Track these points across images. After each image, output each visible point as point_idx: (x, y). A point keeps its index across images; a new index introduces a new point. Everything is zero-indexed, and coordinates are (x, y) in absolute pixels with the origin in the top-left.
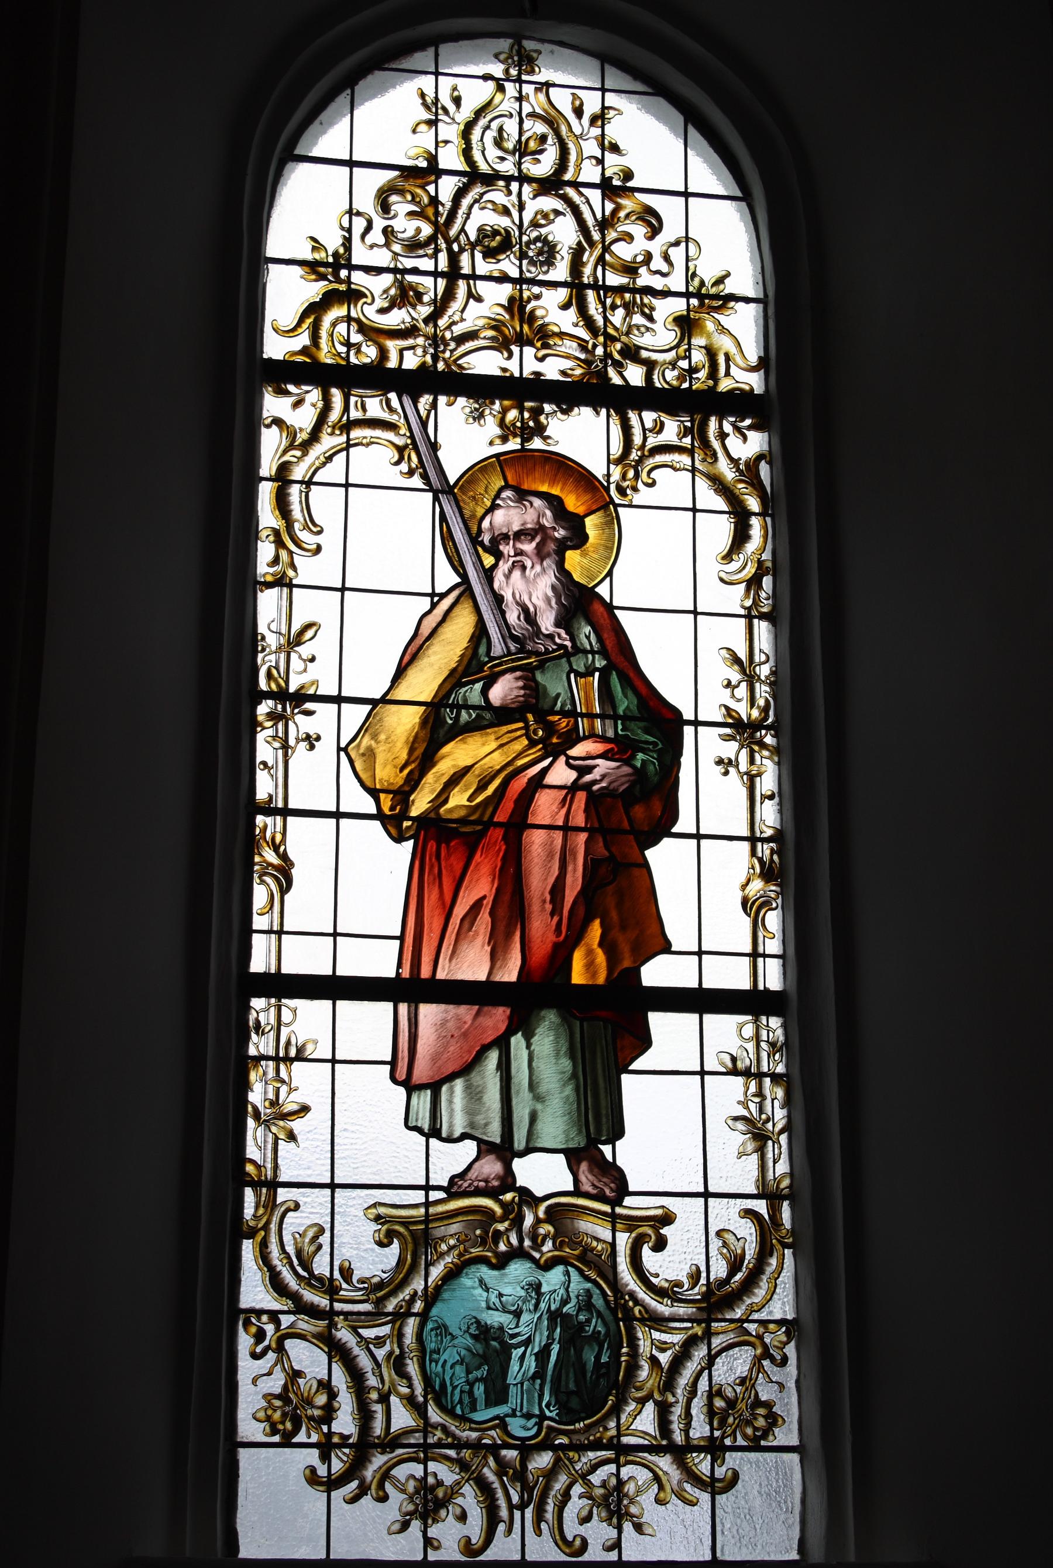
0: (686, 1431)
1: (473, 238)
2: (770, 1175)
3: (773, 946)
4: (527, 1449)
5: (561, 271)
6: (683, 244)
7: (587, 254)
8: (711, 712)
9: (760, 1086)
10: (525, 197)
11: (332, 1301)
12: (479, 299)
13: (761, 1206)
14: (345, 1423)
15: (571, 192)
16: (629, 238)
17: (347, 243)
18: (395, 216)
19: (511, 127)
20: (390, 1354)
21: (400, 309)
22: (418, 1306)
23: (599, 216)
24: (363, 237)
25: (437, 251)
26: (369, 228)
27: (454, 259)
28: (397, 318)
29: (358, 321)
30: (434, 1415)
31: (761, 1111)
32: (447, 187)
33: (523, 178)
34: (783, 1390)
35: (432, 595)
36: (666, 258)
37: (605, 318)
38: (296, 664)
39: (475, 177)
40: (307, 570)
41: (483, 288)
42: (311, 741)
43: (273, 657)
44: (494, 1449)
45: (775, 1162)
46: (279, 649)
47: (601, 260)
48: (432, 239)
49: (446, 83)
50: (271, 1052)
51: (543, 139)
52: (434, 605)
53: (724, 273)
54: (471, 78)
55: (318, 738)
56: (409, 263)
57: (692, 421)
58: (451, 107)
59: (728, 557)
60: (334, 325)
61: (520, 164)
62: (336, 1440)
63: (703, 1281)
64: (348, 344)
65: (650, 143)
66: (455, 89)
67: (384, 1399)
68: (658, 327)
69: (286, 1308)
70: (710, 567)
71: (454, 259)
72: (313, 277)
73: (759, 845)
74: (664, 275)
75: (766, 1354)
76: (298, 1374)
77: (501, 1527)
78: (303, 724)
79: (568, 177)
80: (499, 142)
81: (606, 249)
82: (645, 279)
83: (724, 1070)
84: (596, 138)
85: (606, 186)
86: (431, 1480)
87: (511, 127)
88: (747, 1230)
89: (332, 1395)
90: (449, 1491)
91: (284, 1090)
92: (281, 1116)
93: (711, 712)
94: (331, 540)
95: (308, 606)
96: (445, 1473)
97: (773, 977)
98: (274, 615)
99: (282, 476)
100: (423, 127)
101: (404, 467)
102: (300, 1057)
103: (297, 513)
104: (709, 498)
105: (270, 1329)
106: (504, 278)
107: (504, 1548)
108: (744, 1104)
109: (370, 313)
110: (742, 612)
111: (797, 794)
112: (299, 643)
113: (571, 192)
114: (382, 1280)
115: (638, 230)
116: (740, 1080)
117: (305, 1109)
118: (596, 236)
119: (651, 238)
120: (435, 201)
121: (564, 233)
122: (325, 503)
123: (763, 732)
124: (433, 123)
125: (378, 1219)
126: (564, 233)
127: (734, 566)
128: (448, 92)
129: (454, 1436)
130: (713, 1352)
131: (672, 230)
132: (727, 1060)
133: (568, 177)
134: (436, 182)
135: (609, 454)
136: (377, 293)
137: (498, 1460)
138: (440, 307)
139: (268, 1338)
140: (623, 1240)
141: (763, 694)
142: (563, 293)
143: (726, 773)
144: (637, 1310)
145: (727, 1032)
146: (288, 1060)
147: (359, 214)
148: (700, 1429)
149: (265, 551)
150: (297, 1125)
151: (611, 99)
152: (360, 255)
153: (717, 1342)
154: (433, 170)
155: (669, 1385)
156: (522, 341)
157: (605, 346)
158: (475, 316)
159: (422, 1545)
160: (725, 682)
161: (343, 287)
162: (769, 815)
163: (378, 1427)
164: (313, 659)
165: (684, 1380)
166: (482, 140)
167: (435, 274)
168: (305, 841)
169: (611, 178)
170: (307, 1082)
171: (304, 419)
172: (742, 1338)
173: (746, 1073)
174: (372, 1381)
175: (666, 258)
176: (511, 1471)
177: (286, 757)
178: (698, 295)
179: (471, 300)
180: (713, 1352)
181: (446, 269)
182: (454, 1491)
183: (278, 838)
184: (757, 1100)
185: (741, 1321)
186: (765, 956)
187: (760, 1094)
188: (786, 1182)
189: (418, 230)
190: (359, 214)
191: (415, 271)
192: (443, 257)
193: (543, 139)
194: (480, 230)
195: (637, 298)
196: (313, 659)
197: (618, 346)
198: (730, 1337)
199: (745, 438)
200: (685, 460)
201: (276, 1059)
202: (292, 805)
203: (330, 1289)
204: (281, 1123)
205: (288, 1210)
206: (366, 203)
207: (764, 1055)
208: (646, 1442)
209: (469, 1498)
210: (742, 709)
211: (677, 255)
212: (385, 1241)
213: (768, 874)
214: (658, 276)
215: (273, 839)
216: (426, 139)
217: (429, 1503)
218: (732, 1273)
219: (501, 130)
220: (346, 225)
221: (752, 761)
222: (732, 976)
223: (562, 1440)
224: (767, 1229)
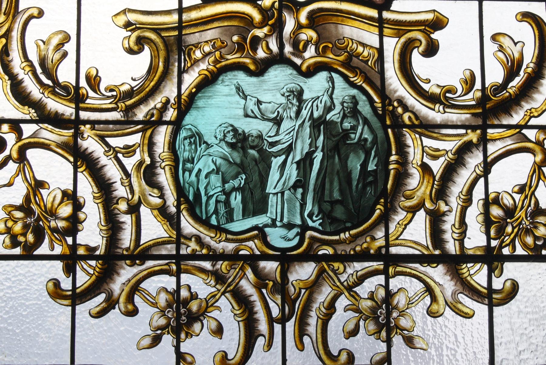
0: (461, 242)
20: (141, 163)
30: (188, 225)
44: (252, 260)
62: (81, 251)
67: (134, 209)
76: (40, 184)
77: (260, 342)
86: (184, 293)
89: (78, 206)
96: (199, 285)
114: (132, 88)
125: (128, 25)
130: (489, 160)
137: (256, 272)
140: (392, 46)
144: (406, 116)
148: (476, 239)
153: (493, 149)
155: (441, 194)
163: (126, 239)
174: (121, 191)
180: (489, 160)
182: (209, 304)
198: (509, 144)
203: (77, 98)
208: (417, 252)
209: (226, 312)
223: (327, 250)
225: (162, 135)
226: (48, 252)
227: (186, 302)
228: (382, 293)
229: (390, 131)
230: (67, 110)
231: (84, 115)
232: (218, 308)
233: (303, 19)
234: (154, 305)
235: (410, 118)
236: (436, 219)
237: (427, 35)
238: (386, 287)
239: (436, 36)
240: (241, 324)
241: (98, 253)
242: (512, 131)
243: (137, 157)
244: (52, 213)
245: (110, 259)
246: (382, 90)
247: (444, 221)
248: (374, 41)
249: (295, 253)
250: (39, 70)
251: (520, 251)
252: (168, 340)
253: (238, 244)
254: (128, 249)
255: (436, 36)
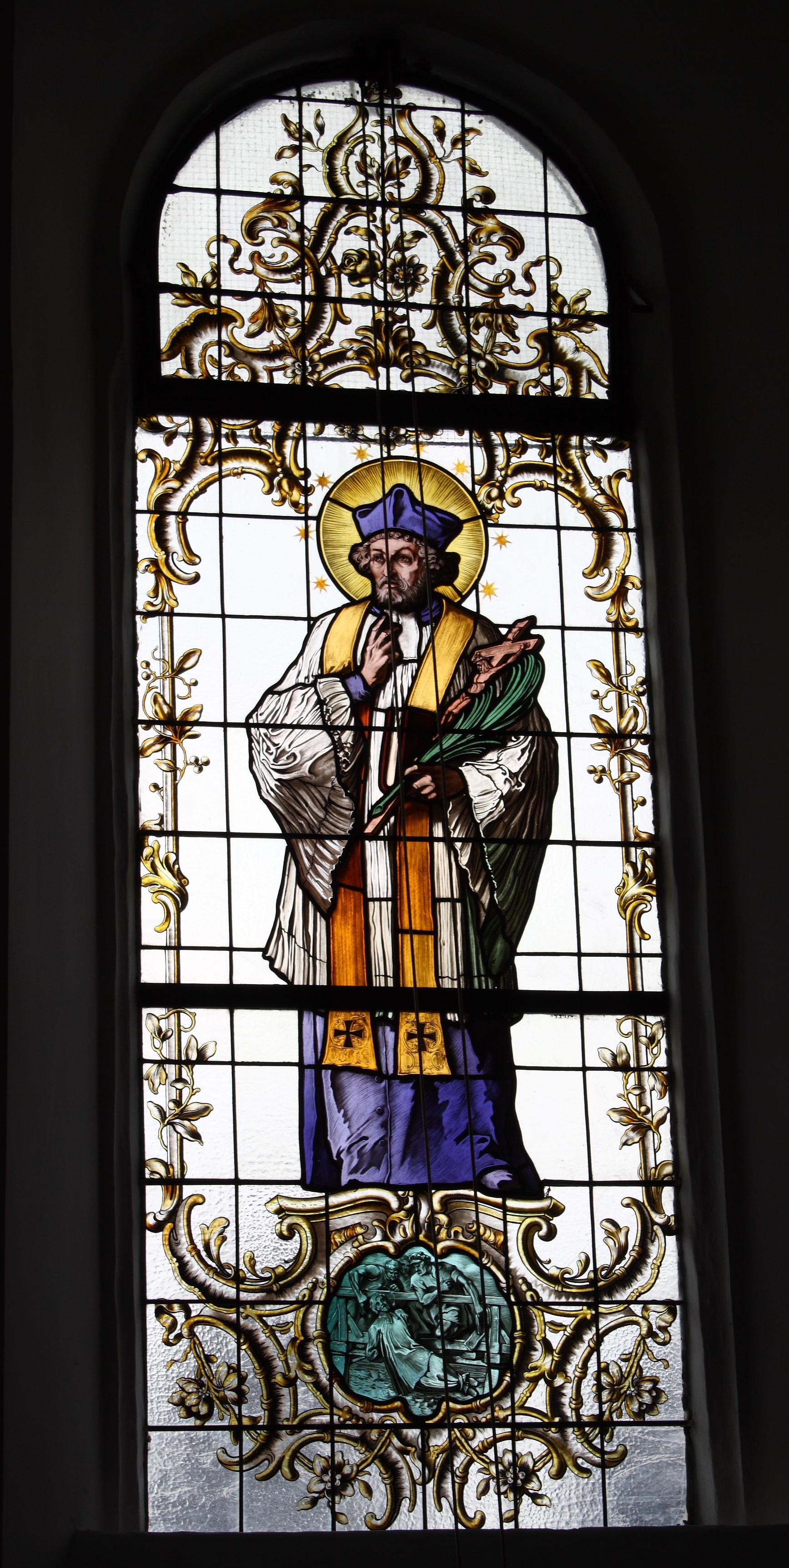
0: (577, 1410)
1: (339, 262)
2: (652, 1164)
3: (653, 945)
4: (427, 1431)
5: (424, 295)
6: (545, 263)
7: (451, 275)
8: (581, 723)
9: (640, 1078)
10: (388, 221)
11: (238, 1290)
12: (346, 322)
13: (638, 1193)
14: (254, 1409)
15: (431, 214)
16: (491, 259)
17: (216, 272)
18: (262, 243)
19: (374, 151)
20: (294, 1340)
21: (269, 331)
22: (320, 1295)
23: (461, 237)
24: (232, 262)
25: (304, 275)
26: (238, 251)
27: (320, 283)
28: (266, 340)
29: (230, 346)
30: (339, 1395)
31: (641, 1103)
32: (312, 213)
33: (386, 205)
34: (667, 1366)
35: (309, 618)
36: (528, 277)
37: (469, 338)
38: (181, 689)
39: (337, 201)
40: (186, 597)
41: (349, 310)
42: (200, 765)
43: (157, 683)
44: (396, 1429)
45: (655, 1152)
46: (163, 677)
47: (465, 280)
48: (299, 264)
49: (310, 109)
50: (174, 1056)
51: (407, 161)
52: (310, 629)
53: (585, 292)
54: (332, 108)
55: (207, 763)
56: (276, 288)
57: (553, 441)
58: (315, 134)
59: (589, 574)
60: (205, 348)
61: (383, 188)
62: (246, 1422)
63: (591, 1267)
64: (218, 364)
65: (508, 165)
66: (318, 115)
67: (291, 1383)
68: (521, 344)
69: (195, 1298)
70: (576, 584)
71: (320, 283)
72: (184, 302)
73: (633, 850)
74: (528, 294)
75: (651, 1334)
76: (209, 1359)
77: (406, 1504)
78: (189, 748)
79: (431, 200)
80: (362, 167)
81: (469, 268)
82: (507, 299)
83: (605, 1066)
84: (458, 160)
85: (466, 208)
86: (338, 1458)
87: (374, 151)
88: (630, 1220)
89: (242, 1379)
90: (355, 1468)
91: (186, 1092)
92: (184, 1116)
93: (581, 723)
94: (208, 568)
95: (189, 634)
96: (353, 1455)
97: (652, 979)
98: (157, 643)
99: (160, 508)
100: (287, 153)
101: (276, 495)
102: (202, 1059)
103: (174, 543)
104: (572, 515)
105: (180, 1317)
106: (371, 301)
107: (408, 1521)
108: (625, 1097)
109: (239, 335)
110: (610, 625)
111: (672, 800)
112: (181, 670)
113: (431, 214)
114: (286, 1270)
115: (500, 252)
116: (620, 1074)
117: (205, 1110)
118: (459, 257)
119: (513, 257)
120: (300, 227)
121: (427, 253)
122: (201, 532)
123: (634, 741)
124: (297, 150)
125: (280, 1211)
126: (427, 253)
127: (599, 581)
128: (312, 120)
129: (358, 1418)
130: (601, 1331)
131: (533, 250)
132: (609, 1057)
133: (431, 200)
134: (302, 208)
135: (473, 475)
136: (247, 316)
137: (403, 1439)
138: (309, 327)
139: (179, 1327)
140: (515, 1232)
141: (631, 705)
142: (427, 315)
143: (600, 781)
144: (529, 1294)
145: (607, 1032)
146: (189, 1063)
147: (226, 240)
148: (590, 1409)
149: (145, 582)
150: (200, 1125)
151: (472, 121)
152: (229, 281)
153: (603, 1323)
154: (299, 197)
155: (560, 1368)
156: (388, 362)
157: (469, 365)
158: (342, 335)
159: (330, 1519)
160: (595, 693)
161: (214, 312)
162: (644, 821)
163: (286, 1408)
164: (196, 684)
165: (576, 1359)
166: (346, 164)
167: (302, 298)
168: (199, 860)
169: (472, 199)
170: (209, 1084)
171: (179, 450)
172: (627, 1318)
173: (624, 1068)
174: (279, 1365)
175: (528, 277)
176: (413, 1449)
177: (175, 778)
178: (560, 315)
179: (338, 322)
180: (601, 1331)
181: (313, 293)
182: (360, 1469)
183: (172, 858)
184: (637, 1092)
185: (628, 1302)
186: (642, 955)
187: (640, 1086)
188: (669, 1169)
189: (285, 256)
190: (226, 240)
191: (283, 296)
192: (309, 281)
193: (407, 161)
194: (346, 256)
195: (502, 317)
196: (196, 684)
197: (483, 364)
198: (620, 1318)
199: (605, 457)
200: (549, 480)
201: (179, 1062)
202: (643, 952)
203: (238, 1279)
204: (186, 1123)
205: (195, 1204)
206: (233, 229)
207: (643, 1048)
208: (539, 1421)
209: (374, 1476)
210: (612, 719)
211: (538, 274)
212: (285, 1233)
213: (641, 877)
214: (520, 296)
215: (167, 859)
216: (291, 165)
217: (338, 1481)
218: (619, 1260)
219: (364, 155)
220: (214, 251)
221: (623, 770)
222: (609, 977)
223: (461, 1419)
224: (645, 1210)
225: (316, 1312)
226: (219, 1423)
227: (341, 1466)
228: (509, 1457)
229: (515, 1308)
230: (230, 1291)
231: (244, 1296)
232: (369, 1474)
233: (437, 1206)
234: (312, 1469)
235: (532, 1296)
236: (555, 1395)
237: (548, 1221)
238: (513, 1451)
239: (556, 1221)
240: (388, 1486)
241: (261, 1424)
242: (621, 1307)
243: (292, 1333)
244: (221, 1386)
245: (273, 1429)
246: (508, 1272)
247: (564, 1394)
248: (499, 1225)
249: (430, 1422)
250: (204, 1254)
251: (626, 1418)
252: (323, 1502)
253: (382, 1415)
254: (288, 1419)
255: (556, 1221)
